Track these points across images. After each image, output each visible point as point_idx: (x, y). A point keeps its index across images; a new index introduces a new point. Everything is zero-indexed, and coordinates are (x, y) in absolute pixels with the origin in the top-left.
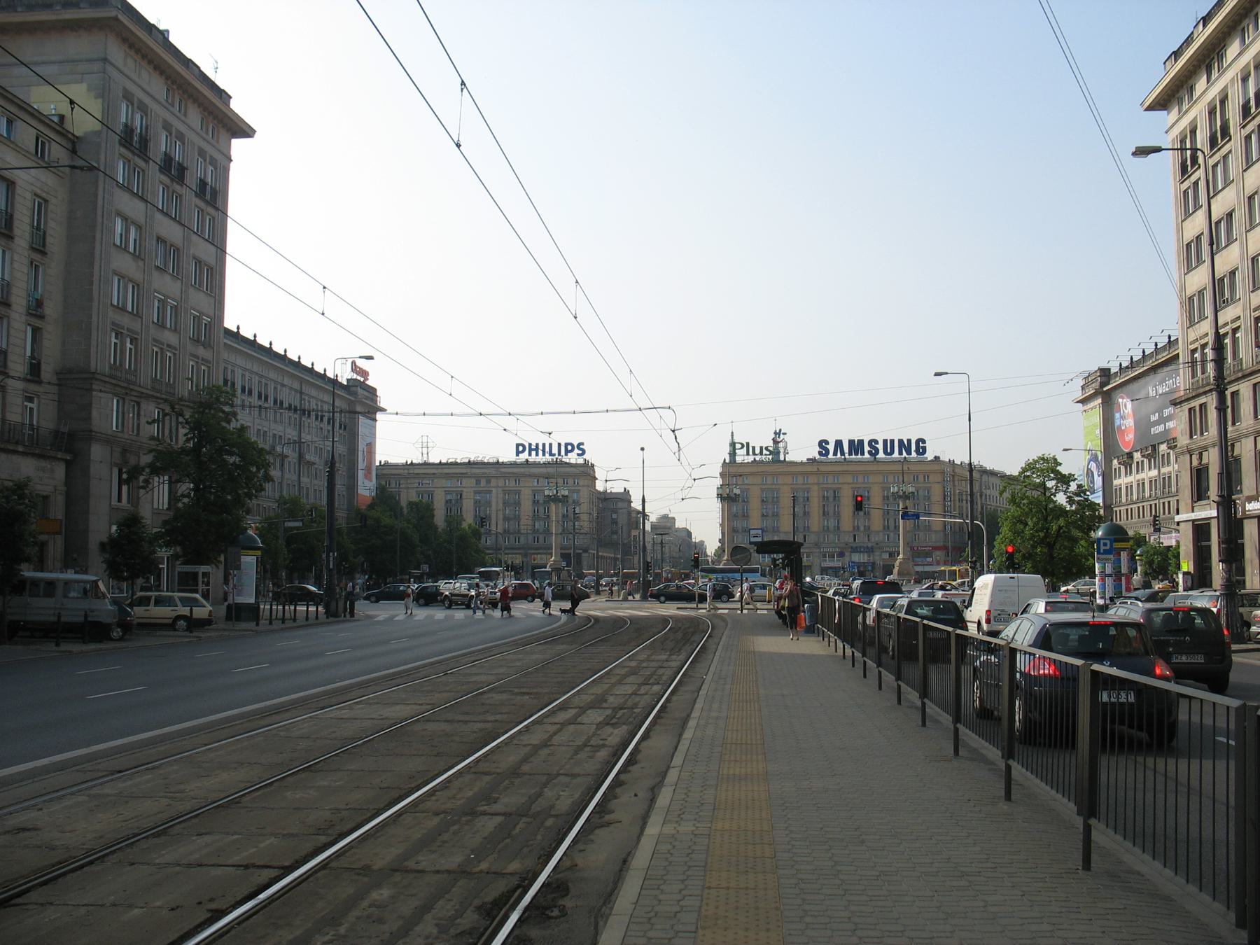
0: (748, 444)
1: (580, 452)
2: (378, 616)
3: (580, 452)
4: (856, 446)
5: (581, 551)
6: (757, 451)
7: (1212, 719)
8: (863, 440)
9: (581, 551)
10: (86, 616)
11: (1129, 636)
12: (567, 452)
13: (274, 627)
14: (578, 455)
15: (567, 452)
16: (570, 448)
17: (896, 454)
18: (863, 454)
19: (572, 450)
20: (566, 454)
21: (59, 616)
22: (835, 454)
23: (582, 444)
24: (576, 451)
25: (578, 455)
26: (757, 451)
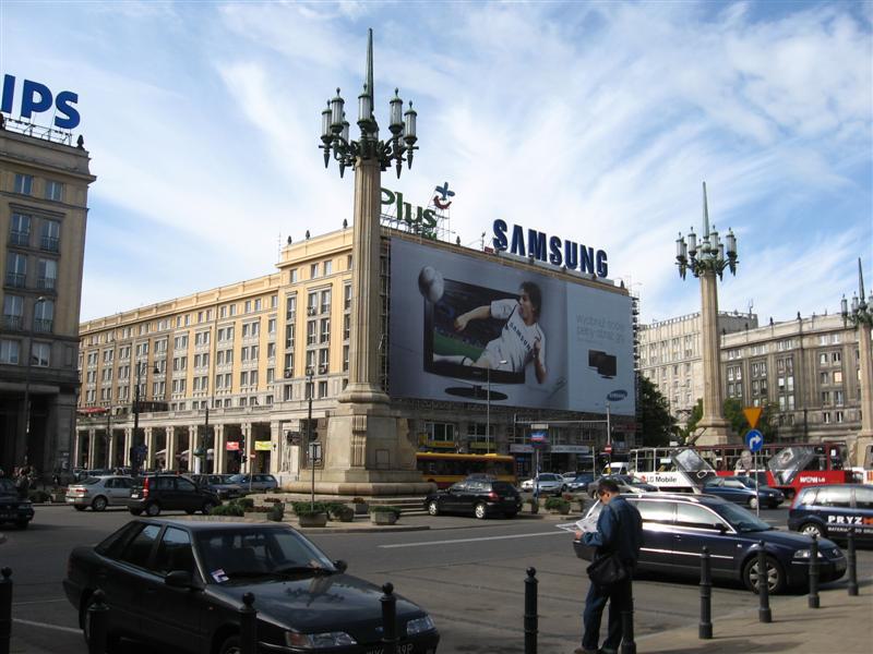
0: (400, 195)
1: (64, 116)
2: (454, 483)
3: (64, 116)
4: (537, 239)
5: (56, 389)
6: (414, 216)
7: (542, 626)
8: (544, 235)
9: (56, 389)
10: (815, 603)
11: (232, 543)
12: (28, 109)
13: (680, 348)
14: (59, 122)
15: (28, 109)
16: (37, 98)
17: (578, 269)
18: (545, 259)
19: (43, 107)
20: (26, 112)
21: (815, 603)
22: (514, 250)
23: (74, 98)
24: (54, 111)
25: (59, 122)
26: (414, 216)
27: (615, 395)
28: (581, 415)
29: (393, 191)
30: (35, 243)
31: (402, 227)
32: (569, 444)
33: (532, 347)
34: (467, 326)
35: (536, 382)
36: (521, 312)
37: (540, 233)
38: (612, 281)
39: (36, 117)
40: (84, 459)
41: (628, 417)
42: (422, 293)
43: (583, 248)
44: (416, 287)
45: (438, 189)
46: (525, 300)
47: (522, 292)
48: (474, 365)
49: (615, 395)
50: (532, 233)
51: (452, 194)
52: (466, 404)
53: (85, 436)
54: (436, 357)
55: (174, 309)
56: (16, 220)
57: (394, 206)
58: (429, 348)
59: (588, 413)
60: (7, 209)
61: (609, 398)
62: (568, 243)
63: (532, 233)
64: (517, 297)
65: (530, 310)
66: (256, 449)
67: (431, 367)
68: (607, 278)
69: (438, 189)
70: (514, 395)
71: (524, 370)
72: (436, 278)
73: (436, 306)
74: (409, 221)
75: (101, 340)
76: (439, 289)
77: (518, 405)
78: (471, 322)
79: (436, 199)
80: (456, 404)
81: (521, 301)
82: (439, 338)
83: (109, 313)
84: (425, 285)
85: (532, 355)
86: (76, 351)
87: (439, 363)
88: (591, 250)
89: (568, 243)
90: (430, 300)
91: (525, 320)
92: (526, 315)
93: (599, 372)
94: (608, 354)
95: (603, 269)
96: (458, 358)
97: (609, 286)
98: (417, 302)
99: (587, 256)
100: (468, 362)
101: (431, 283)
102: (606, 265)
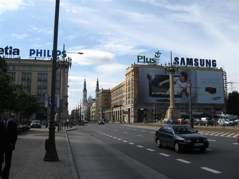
0: (144, 57)
4: (190, 61)
6: (149, 60)
17: (205, 66)
18: (192, 65)
26: (149, 60)
27: (216, 98)
28: (202, 104)
29: (142, 56)
30: (27, 78)
31: (147, 64)
32: (200, 112)
33: (184, 88)
34: (162, 85)
35: (186, 96)
36: (180, 80)
37: (190, 59)
38: (217, 68)
39: (32, 56)
40: (109, 119)
41: (223, 104)
42: (148, 79)
43: (207, 60)
44: (146, 78)
45: (156, 53)
46: (181, 76)
47: (181, 75)
48: (165, 94)
49: (216, 98)
50: (188, 59)
51: (160, 54)
52: (162, 104)
53: (114, 112)
54: (153, 93)
55: (123, 84)
56: (23, 75)
57: (143, 59)
58: (151, 91)
59: (205, 104)
60: (37, 74)
61: (213, 99)
62: (201, 60)
63: (188, 59)
64: (179, 76)
65: (183, 79)
66: (193, 114)
67: (151, 95)
68: (216, 67)
69: (156, 53)
70: (38, 107)
71: (181, 94)
72: (152, 75)
73: (153, 81)
74: (147, 62)
75: (115, 92)
76: (153, 77)
77: (180, 103)
78: (163, 84)
79: (155, 56)
80: (160, 104)
81: (180, 77)
82: (153, 88)
83: (114, 87)
84: (149, 77)
85: (185, 90)
86: (110, 95)
87: (153, 94)
88: (210, 60)
89: (201, 60)
90: (150, 80)
91: (182, 82)
92: (182, 80)
93: (209, 93)
94: (213, 87)
95: (215, 65)
96: (160, 93)
97: (217, 70)
98: (147, 81)
99: (208, 62)
100: (163, 93)
101: (151, 76)
102: (216, 64)
